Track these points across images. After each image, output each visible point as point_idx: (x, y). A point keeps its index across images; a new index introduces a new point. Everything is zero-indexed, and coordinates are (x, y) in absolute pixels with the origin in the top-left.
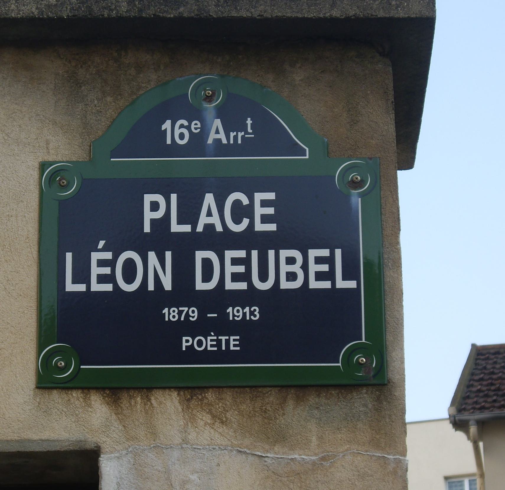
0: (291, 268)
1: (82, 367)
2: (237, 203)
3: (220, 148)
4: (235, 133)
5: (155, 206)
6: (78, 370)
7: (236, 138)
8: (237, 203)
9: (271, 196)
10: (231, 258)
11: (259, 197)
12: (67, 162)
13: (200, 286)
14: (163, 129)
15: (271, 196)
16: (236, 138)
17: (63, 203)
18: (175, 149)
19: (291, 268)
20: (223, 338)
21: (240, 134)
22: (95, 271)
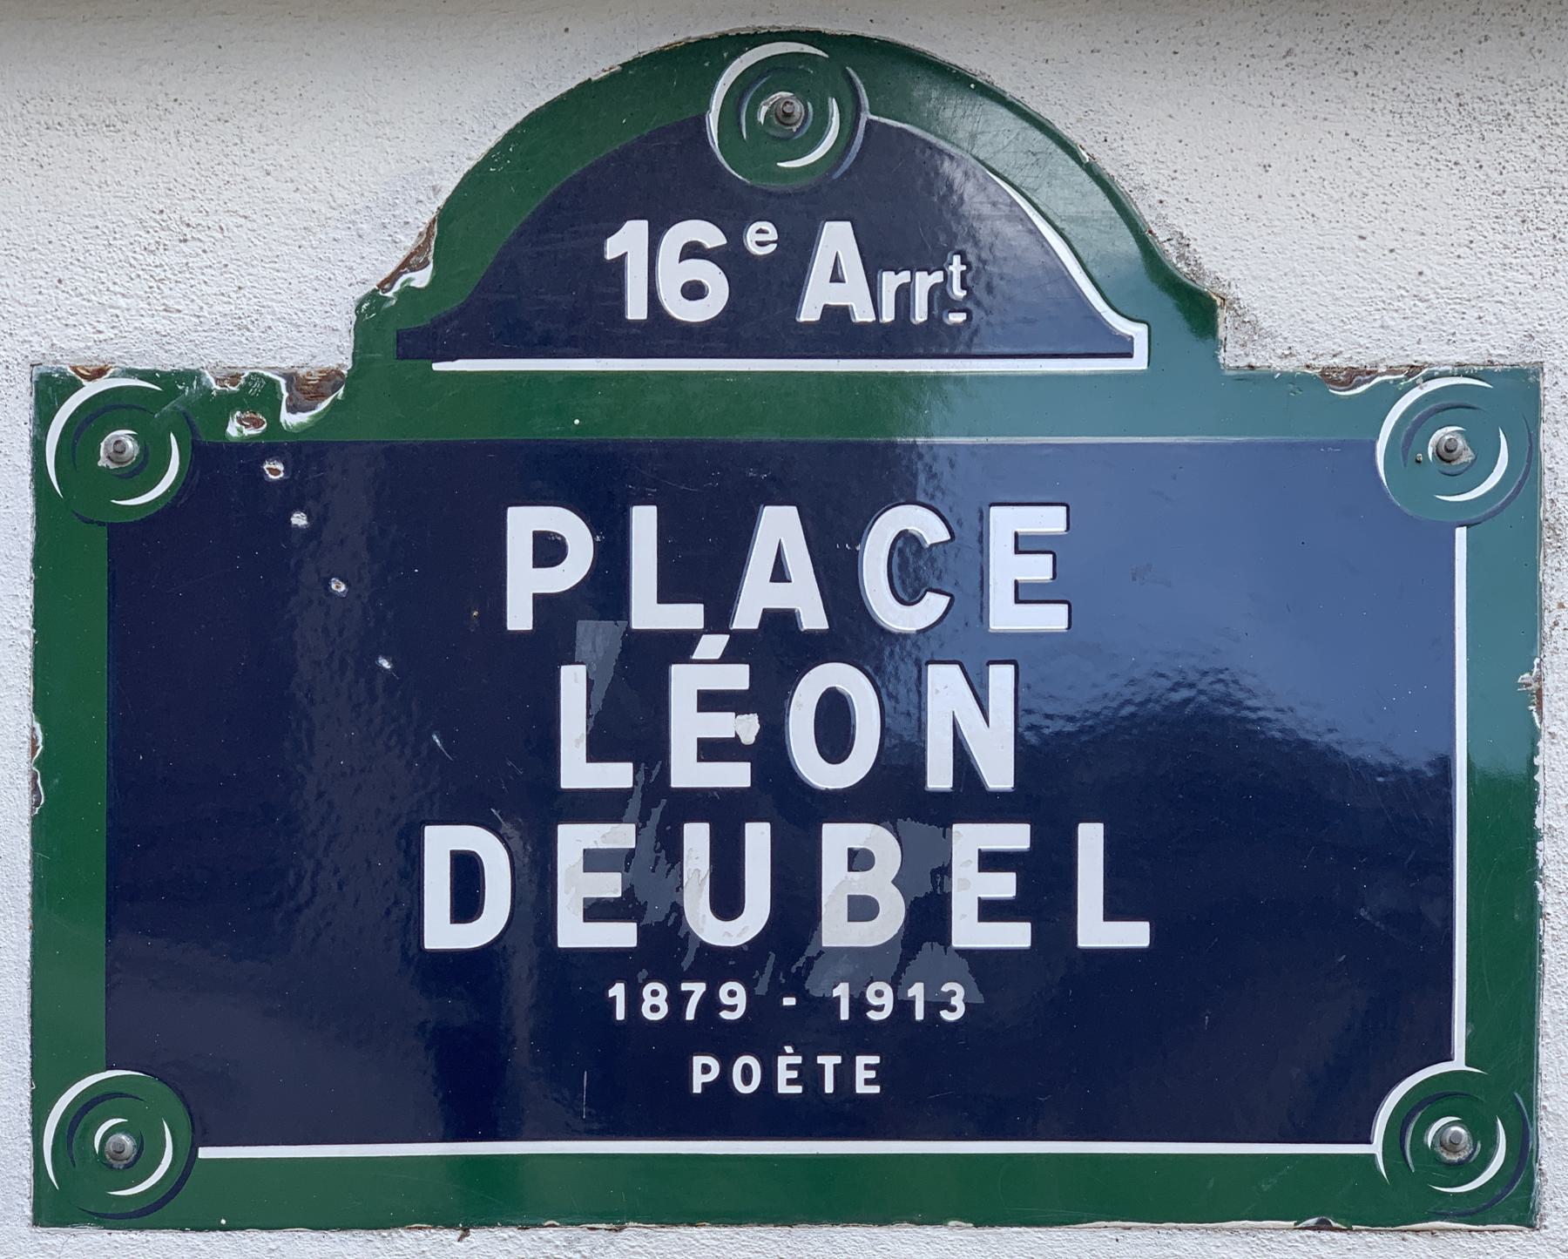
0: (862, 884)
1: (205, 1153)
2: (906, 542)
3: (837, 333)
4: (905, 277)
5: (549, 550)
6: (187, 1163)
7: (904, 295)
8: (906, 542)
9: (1051, 520)
10: (453, 853)
11: (1005, 523)
12: (130, 373)
13: (442, 932)
14: (609, 257)
15: (1051, 520)
16: (904, 295)
17: (130, 539)
18: (662, 333)
19: (862, 884)
20: (829, 1062)
21: (924, 282)
22: (687, 725)
